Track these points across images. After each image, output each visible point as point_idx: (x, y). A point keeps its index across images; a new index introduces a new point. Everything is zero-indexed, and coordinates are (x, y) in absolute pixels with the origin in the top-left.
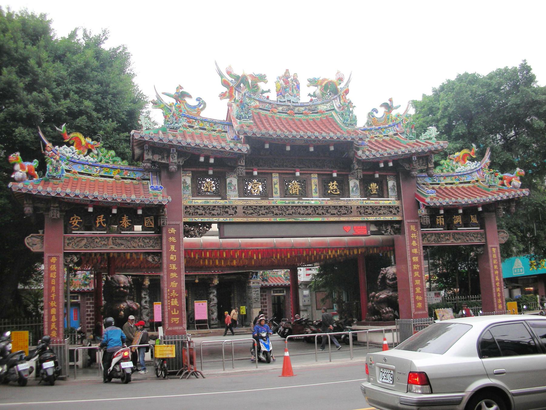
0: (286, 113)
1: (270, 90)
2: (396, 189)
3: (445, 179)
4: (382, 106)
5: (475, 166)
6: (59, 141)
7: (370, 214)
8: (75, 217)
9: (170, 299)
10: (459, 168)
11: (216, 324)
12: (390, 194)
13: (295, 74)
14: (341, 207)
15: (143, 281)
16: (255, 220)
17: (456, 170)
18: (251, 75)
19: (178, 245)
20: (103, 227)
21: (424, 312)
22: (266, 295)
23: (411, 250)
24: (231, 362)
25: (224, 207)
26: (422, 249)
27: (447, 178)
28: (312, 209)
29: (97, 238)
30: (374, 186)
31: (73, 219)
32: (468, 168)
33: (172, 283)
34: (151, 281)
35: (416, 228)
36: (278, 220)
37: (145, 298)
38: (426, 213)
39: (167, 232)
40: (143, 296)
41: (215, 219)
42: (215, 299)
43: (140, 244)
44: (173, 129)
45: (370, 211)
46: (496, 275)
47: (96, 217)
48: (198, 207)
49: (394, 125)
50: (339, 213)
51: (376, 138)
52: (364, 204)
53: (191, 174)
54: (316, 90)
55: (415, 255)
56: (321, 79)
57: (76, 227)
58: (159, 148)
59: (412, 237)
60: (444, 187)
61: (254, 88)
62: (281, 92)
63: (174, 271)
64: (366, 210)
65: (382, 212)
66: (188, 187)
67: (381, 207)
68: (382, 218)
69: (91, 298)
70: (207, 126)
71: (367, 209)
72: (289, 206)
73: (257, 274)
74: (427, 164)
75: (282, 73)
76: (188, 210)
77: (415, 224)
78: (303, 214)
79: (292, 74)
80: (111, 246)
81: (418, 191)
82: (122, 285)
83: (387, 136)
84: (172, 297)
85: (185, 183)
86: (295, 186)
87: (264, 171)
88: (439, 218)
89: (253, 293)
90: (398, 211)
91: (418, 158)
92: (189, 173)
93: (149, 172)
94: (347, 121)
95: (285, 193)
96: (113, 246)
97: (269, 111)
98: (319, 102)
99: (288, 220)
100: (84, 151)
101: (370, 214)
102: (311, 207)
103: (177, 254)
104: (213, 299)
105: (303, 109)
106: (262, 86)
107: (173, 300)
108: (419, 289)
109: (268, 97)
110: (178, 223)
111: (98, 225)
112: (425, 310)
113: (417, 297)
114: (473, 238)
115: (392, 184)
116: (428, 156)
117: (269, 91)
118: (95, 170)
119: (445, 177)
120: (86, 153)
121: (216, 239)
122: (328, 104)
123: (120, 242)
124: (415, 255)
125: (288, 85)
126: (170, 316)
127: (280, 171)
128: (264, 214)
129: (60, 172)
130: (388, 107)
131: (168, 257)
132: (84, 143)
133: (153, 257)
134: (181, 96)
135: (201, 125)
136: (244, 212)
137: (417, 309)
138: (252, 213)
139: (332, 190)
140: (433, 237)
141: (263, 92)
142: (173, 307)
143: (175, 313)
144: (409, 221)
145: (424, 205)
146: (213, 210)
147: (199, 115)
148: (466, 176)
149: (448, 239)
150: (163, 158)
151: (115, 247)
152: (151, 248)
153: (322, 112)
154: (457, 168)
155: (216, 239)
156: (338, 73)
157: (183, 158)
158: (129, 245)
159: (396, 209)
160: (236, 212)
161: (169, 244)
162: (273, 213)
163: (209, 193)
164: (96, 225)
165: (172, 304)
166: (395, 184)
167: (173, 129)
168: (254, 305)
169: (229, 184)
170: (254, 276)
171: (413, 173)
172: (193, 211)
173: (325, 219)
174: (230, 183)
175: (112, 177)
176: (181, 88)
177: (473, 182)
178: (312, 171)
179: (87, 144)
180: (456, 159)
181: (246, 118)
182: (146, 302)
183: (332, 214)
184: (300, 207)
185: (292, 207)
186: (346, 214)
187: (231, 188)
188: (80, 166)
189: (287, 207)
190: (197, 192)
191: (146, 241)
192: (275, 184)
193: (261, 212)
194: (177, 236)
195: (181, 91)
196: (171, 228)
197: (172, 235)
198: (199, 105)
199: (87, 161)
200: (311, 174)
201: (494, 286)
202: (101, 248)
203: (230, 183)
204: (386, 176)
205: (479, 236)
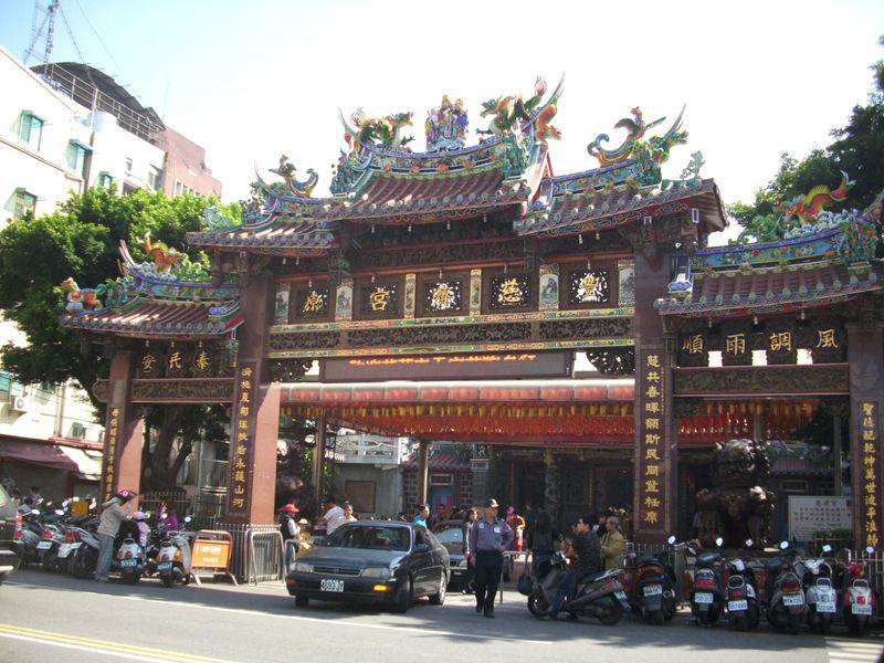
1: (416, 139)
5: (840, 221)
14: (510, 325)
17: (787, 235)
29: (165, 384)
32: (821, 226)
34: (555, 457)
52: (557, 318)
62: (434, 133)
66: (284, 306)
67: (590, 321)
68: (591, 342)
71: (561, 326)
84: (237, 469)
88: (730, 339)
97: (407, 171)
102: (457, 327)
139: (507, 295)
143: (239, 492)
156: (538, 81)
160: (338, 341)
174: (342, 296)
178: (471, 264)
182: (550, 492)
183: (492, 339)
184: (437, 328)
185: (425, 328)
204: (617, 259)
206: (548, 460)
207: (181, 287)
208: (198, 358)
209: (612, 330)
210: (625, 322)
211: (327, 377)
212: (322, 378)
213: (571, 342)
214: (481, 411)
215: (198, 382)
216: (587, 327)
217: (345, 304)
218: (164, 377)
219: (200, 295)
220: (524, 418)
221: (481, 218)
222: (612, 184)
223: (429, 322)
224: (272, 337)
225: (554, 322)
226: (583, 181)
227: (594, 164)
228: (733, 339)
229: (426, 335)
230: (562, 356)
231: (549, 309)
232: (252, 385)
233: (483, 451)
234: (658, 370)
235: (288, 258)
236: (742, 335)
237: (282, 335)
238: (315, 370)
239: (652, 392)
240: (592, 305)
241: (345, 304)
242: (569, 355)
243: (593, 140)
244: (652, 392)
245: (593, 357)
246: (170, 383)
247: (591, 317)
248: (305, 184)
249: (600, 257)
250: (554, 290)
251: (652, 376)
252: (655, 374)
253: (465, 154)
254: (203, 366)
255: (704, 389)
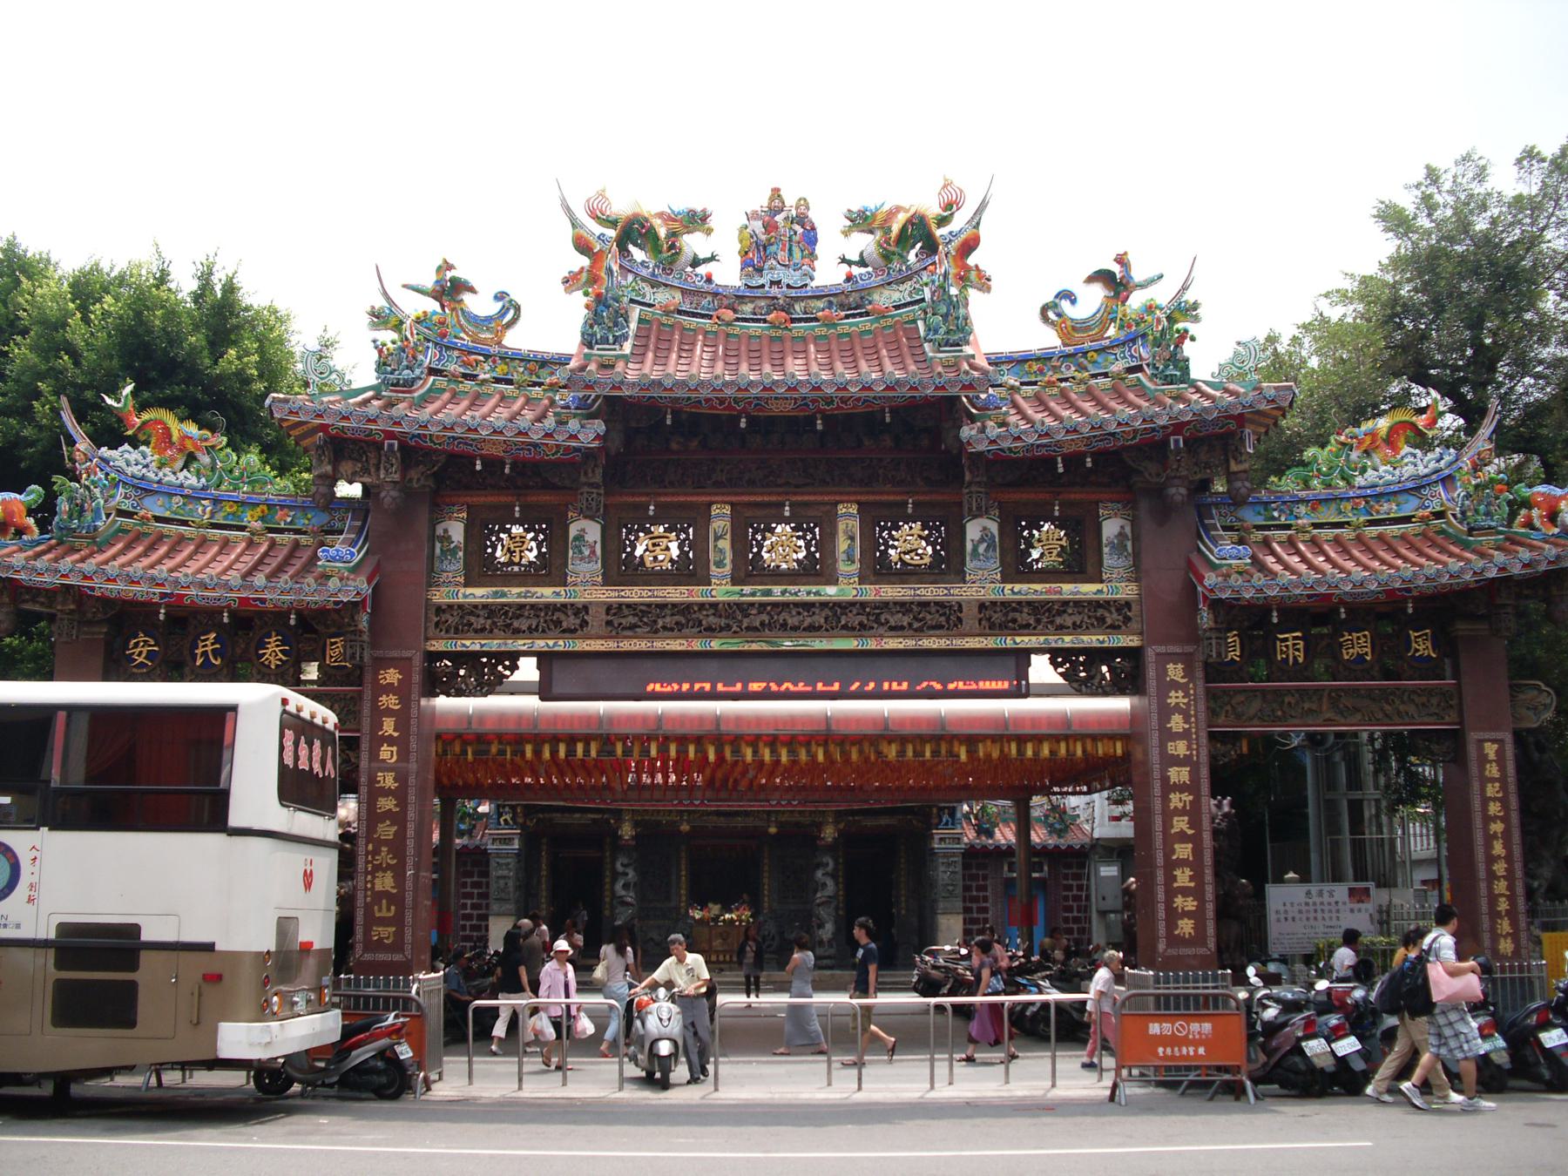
2: (1129, 544)
3: (1314, 509)
4: (1091, 279)
5: (1433, 465)
6: (110, 433)
7: (1027, 626)
8: (142, 637)
9: (373, 873)
10: (1370, 472)
11: (829, 957)
13: (803, 203)
15: (819, 826)
16: (641, 645)
17: (1359, 481)
18: (660, 215)
21: (1202, 951)
22: (985, 878)
25: (1095, 605)
27: (1322, 509)
28: (827, 612)
31: (136, 645)
32: (1408, 471)
34: (636, 824)
35: (1188, 672)
36: (715, 645)
39: (376, 680)
40: (619, 868)
42: (830, 882)
44: (397, 385)
45: (1024, 617)
46: (1495, 836)
49: (1133, 341)
50: (916, 625)
54: (864, 243)
55: (1177, 761)
56: (886, 208)
57: (142, 665)
58: (355, 441)
59: (1172, 701)
61: (668, 255)
63: (387, 793)
65: (523, 624)
66: (454, 552)
68: (1067, 639)
71: (1014, 610)
75: (761, 201)
77: (1187, 660)
79: (790, 200)
83: (1106, 375)
85: (449, 539)
86: (1046, 542)
89: (942, 868)
92: (459, 511)
95: (1016, 567)
97: (710, 317)
98: (876, 280)
100: (173, 459)
101: (1027, 626)
104: (824, 885)
105: (820, 304)
106: (694, 243)
108: (1188, 872)
109: (709, 280)
112: (1204, 944)
113: (1179, 901)
114: (1412, 709)
115: (1116, 530)
117: (713, 258)
119: (1316, 503)
120: (180, 464)
121: (531, 703)
122: (908, 286)
124: (1177, 761)
125: (781, 233)
126: (371, 921)
128: (672, 630)
129: (88, 516)
132: (175, 437)
134: (450, 290)
135: (501, 370)
136: (609, 623)
137: (1174, 941)
138: (633, 627)
141: (696, 262)
142: (379, 896)
143: (384, 914)
144: (1162, 649)
147: (499, 343)
148: (1401, 498)
149: (1310, 710)
153: (882, 314)
154: (1363, 470)
155: (531, 703)
156: (945, 186)
159: (1119, 610)
162: (700, 624)
163: (516, 569)
164: (195, 661)
165: (378, 887)
166: (1128, 530)
168: (941, 905)
169: (576, 539)
171: (1173, 491)
173: (872, 644)
174: (580, 538)
175: (242, 528)
176: (450, 267)
177: (1423, 519)
178: (841, 494)
179: (185, 437)
180: (1360, 442)
182: (626, 886)
183: (892, 629)
185: (763, 605)
187: (581, 552)
188: (161, 500)
189: (743, 608)
190: (481, 568)
192: (717, 539)
193: (660, 623)
194: (402, 691)
195: (449, 275)
197: (389, 689)
198: (503, 312)
199: (181, 486)
201: (1482, 874)
203: (580, 538)
205: (1434, 701)
206: (627, 831)
233: (508, 817)
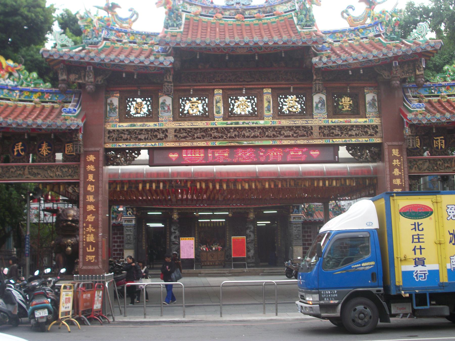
0: (234, 18)
3: (448, 89)
7: (338, 135)
11: (252, 263)
12: (368, 110)
14: (298, 127)
15: (248, 214)
19: (97, 174)
20: (21, 155)
22: (310, 232)
23: (391, 181)
24: (160, 308)
26: (407, 179)
28: (260, 130)
30: (346, 102)
33: (88, 217)
34: (179, 214)
36: (217, 144)
37: (175, 233)
38: (410, 134)
40: (173, 231)
41: (142, 145)
42: (252, 234)
43: (57, 173)
44: (91, 44)
45: (337, 132)
47: (15, 144)
48: (123, 131)
50: (295, 135)
51: (350, 42)
53: (118, 95)
60: (445, 100)
63: (90, 203)
64: (332, 131)
66: (114, 109)
67: (352, 126)
68: (353, 140)
69: (118, 232)
70: (139, 39)
71: (333, 129)
72: (231, 128)
73: (298, 208)
74: (415, 71)
76: (111, 135)
78: (248, 137)
80: (26, 176)
81: (404, 105)
82: (70, 219)
83: (366, 38)
84: (88, 233)
87: (203, 87)
90: (376, 132)
91: (402, 64)
92: (116, 94)
93: (72, 94)
94: (302, 21)
96: (29, 176)
97: (212, 17)
99: (229, 144)
102: (259, 128)
103: (96, 183)
105: (255, 11)
107: (89, 235)
110: (97, 149)
111: (16, 153)
116: (417, 60)
118: (15, 94)
123: (35, 171)
127: (223, 87)
128: (200, 138)
130: (111, 8)
131: (85, 188)
133: (73, 187)
135: (132, 38)
140: (427, 164)
143: (91, 250)
144: (390, 143)
145: (407, 123)
146: (140, 134)
150: (80, 78)
151: (31, 177)
152: (70, 178)
153: (279, 15)
157: (101, 77)
158: (46, 175)
159: (373, 129)
161: (87, 173)
162: (211, 136)
165: (88, 240)
166: (376, 98)
167: (91, 44)
169: (162, 103)
170: (295, 210)
171: (394, 82)
172: (116, 135)
174: (163, 103)
175: (31, 101)
178: (263, 85)
179: (8, 66)
181: (173, 26)
183: (286, 137)
184: (244, 128)
185: (235, 128)
186: (304, 136)
187: (164, 109)
189: (228, 129)
191: (64, 170)
192: (217, 102)
193: (196, 135)
196: (89, 155)
197: (91, 163)
200: (263, 88)
202: (16, 179)
203: (163, 103)
207: (21, 91)
208: (41, 147)
209: (366, 132)
210: (375, 127)
211: (155, 162)
212: (151, 163)
213: (340, 140)
214: (154, 186)
215: (45, 166)
216: (350, 130)
217: (166, 109)
218: (9, 162)
219: (39, 97)
220: (282, 188)
221: (253, 56)
222: (359, 38)
223: (237, 123)
224: (109, 132)
225: (328, 126)
226: (339, 35)
227: (344, 25)
228: (438, 140)
229: (236, 133)
230: (332, 149)
231: (320, 119)
232: (97, 167)
234: (399, 158)
235: (127, 73)
236: (442, 137)
237: (118, 130)
238: (144, 155)
239: (396, 172)
240: (246, 117)
241: (166, 109)
242: (336, 147)
243: (344, 8)
244: (396, 172)
245: (351, 150)
246: (17, 167)
247: (352, 124)
248: (127, 19)
249: (354, 85)
250: (323, 104)
251: (396, 162)
252: (398, 161)
253: (255, 9)
254: (45, 154)
255: (425, 170)
